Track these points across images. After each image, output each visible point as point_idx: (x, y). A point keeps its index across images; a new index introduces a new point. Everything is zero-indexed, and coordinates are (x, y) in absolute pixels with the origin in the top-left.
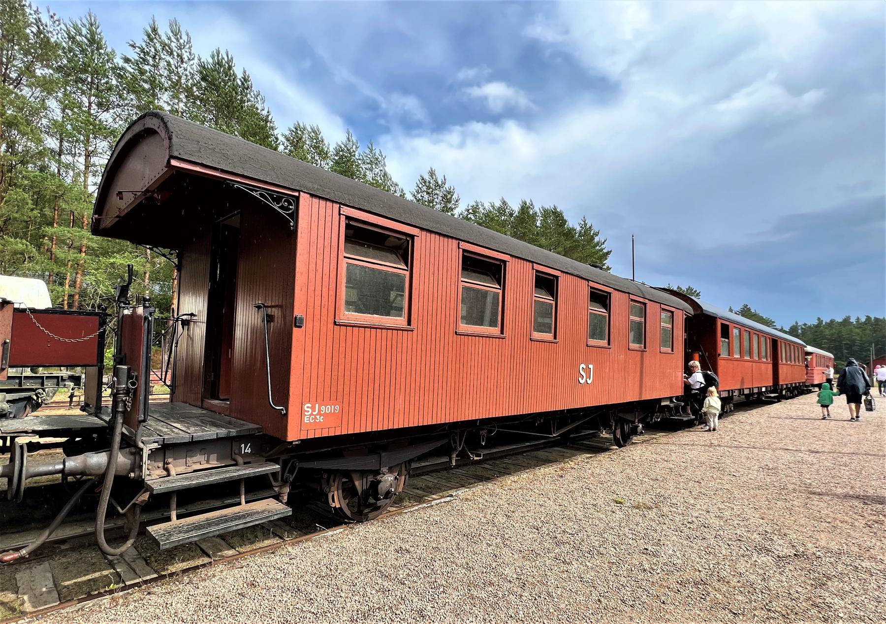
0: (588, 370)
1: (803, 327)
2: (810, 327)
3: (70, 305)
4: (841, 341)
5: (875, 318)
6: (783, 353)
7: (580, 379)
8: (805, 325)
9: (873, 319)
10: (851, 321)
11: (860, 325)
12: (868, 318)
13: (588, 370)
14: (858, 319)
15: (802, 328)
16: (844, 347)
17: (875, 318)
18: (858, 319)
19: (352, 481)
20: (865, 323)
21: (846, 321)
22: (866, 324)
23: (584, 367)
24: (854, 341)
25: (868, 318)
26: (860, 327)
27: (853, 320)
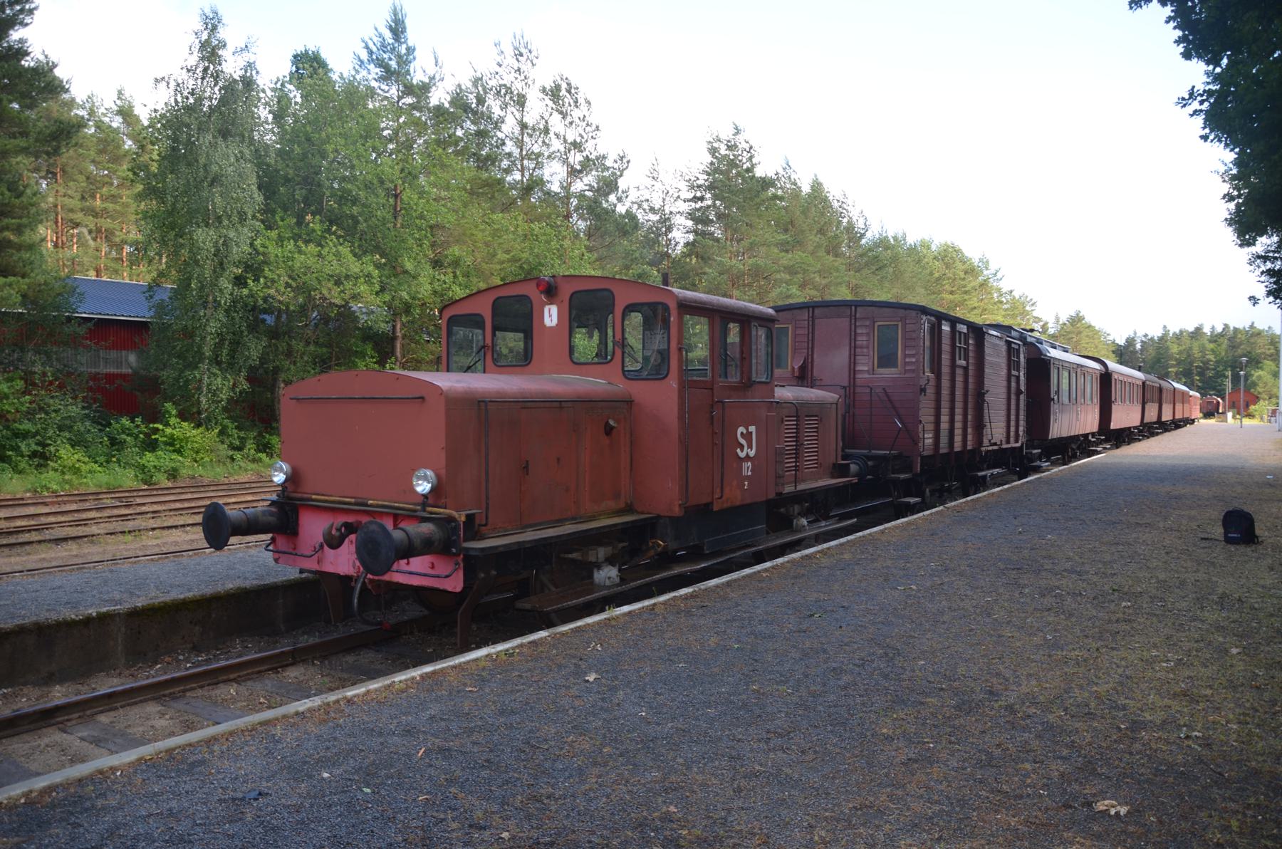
0: (748, 436)
1: (1144, 339)
2: (1152, 339)
3: (177, 105)
4: (1191, 363)
5: (1234, 328)
6: (1116, 392)
7: (738, 450)
8: (1146, 336)
9: (1232, 328)
10: (1234, 207)
11: (1215, 338)
12: (1226, 326)
13: (748, 436)
14: (1213, 328)
15: (1142, 341)
16: (1195, 372)
17: (1234, 328)
18: (1213, 328)
19: (940, 326)
20: (1221, 335)
21: (1198, 331)
22: (1223, 336)
23: (745, 432)
24: (1206, 363)
25: (1226, 326)
26: (1215, 341)
27: (1207, 330)
